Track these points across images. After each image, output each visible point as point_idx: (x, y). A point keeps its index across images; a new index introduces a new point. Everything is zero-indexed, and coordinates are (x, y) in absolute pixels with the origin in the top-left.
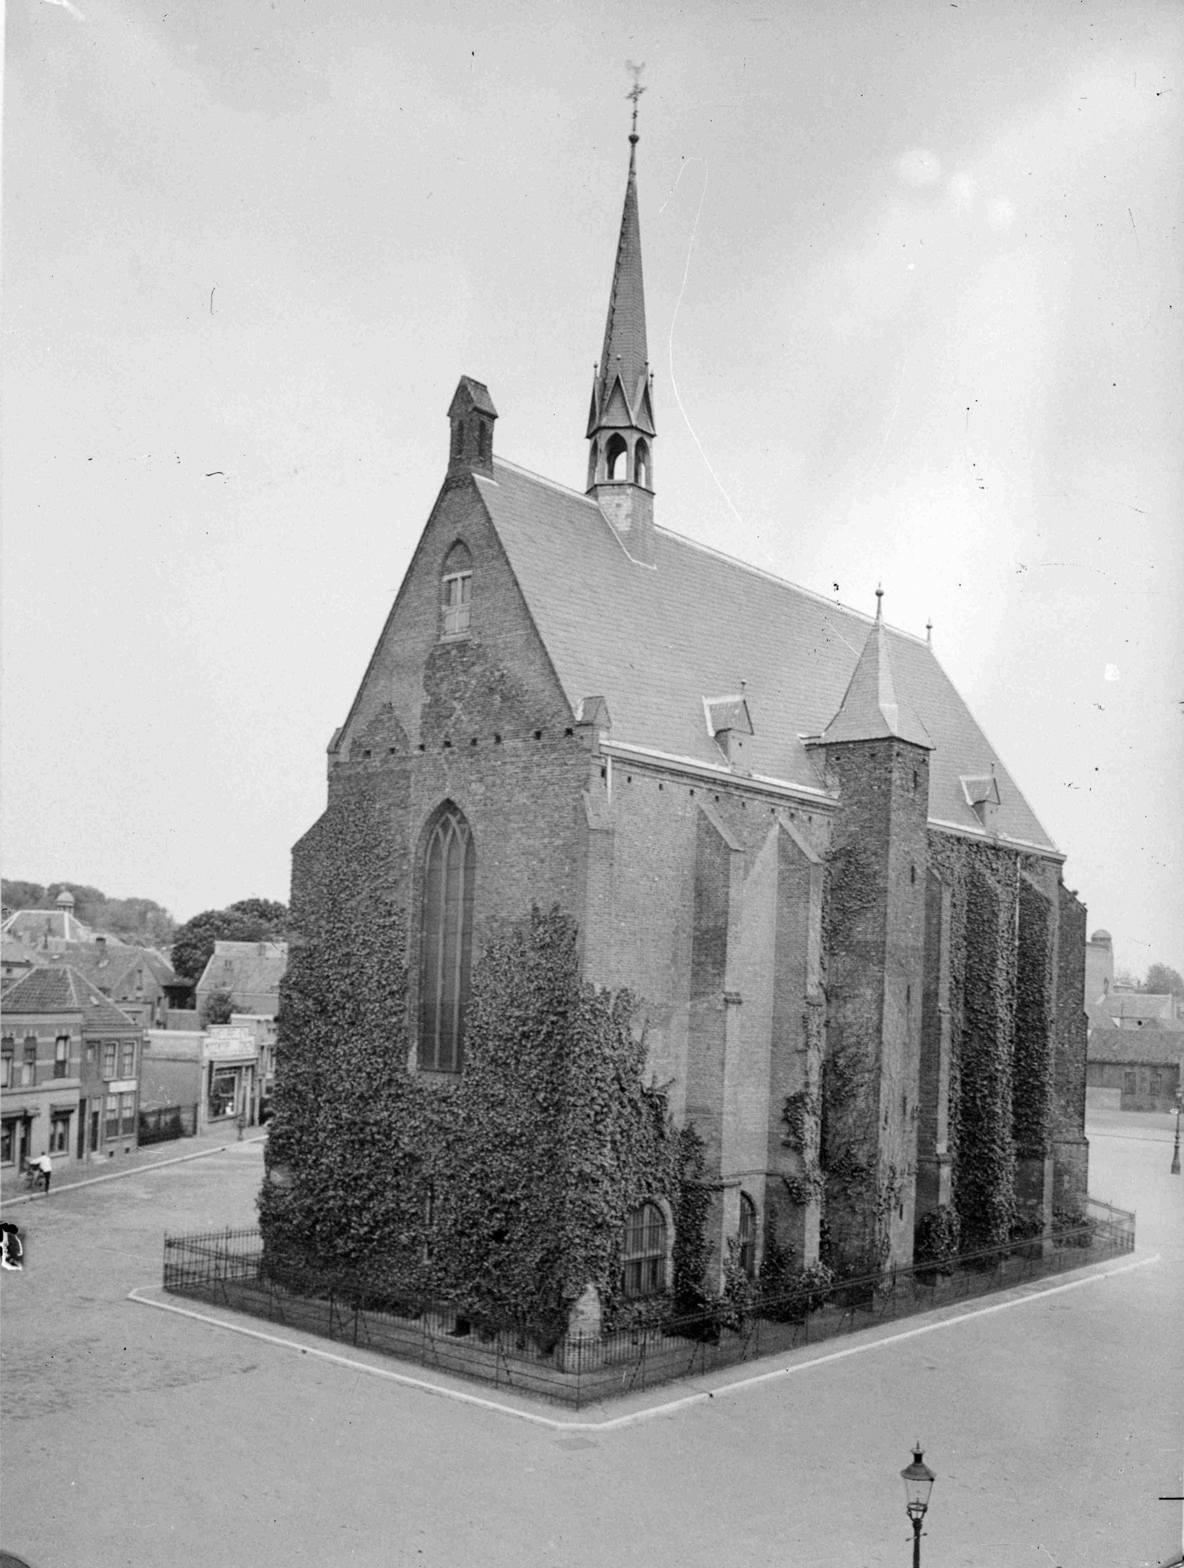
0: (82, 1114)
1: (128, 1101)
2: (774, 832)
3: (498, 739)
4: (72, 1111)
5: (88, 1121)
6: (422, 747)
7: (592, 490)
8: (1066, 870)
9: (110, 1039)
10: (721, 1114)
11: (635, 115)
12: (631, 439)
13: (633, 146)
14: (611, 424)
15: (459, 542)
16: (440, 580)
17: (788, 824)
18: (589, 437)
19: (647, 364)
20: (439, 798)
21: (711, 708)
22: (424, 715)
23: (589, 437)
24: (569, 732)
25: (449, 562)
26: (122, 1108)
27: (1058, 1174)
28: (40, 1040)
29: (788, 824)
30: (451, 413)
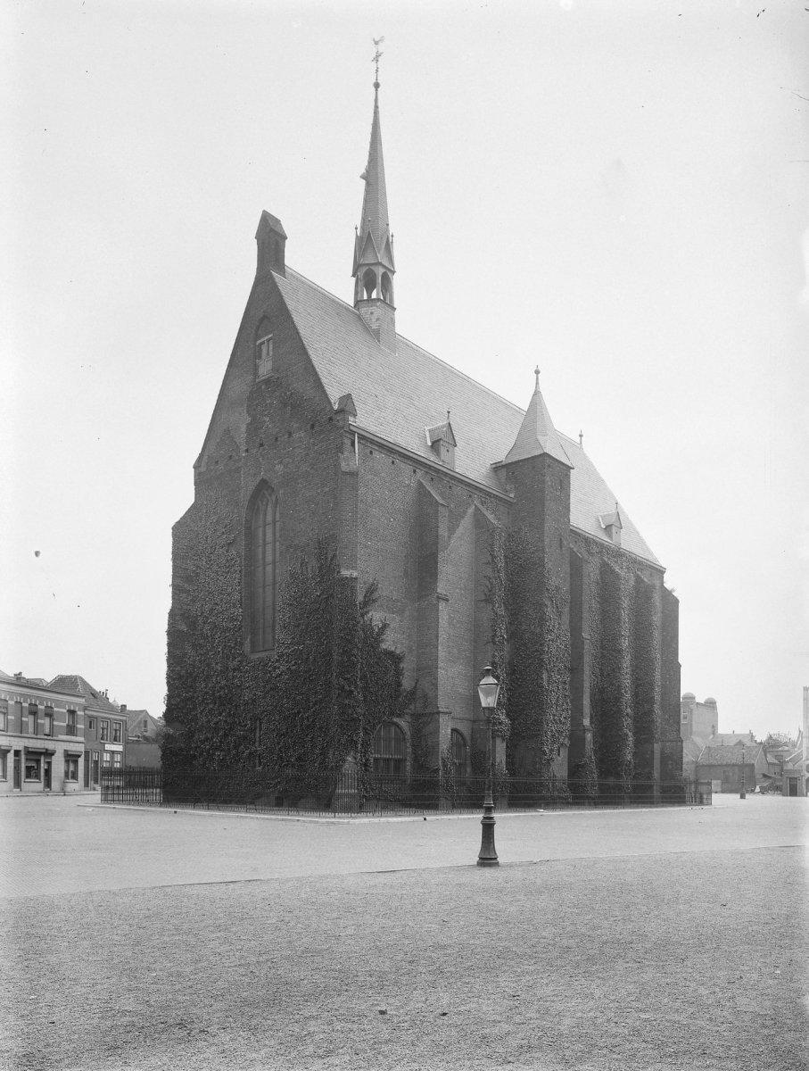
0: (87, 760)
1: (118, 758)
2: (471, 510)
3: (290, 434)
4: (79, 756)
5: (92, 765)
6: (247, 451)
7: (358, 302)
8: (666, 576)
9: (106, 718)
10: (437, 668)
11: (377, 86)
12: (380, 271)
13: (377, 90)
14: (367, 262)
15: (265, 317)
16: (255, 344)
17: (480, 506)
18: (353, 276)
19: (388, 225)
20: (259, 479)
21: (430, 431)
22: (248, 430)
23: (353, 276)
24: (331, 419)
25: (260, 332)
26: (112, 761)
27: (664, 759)
28: (55, 709)
29: (480, 506)
30: (258, 237)
